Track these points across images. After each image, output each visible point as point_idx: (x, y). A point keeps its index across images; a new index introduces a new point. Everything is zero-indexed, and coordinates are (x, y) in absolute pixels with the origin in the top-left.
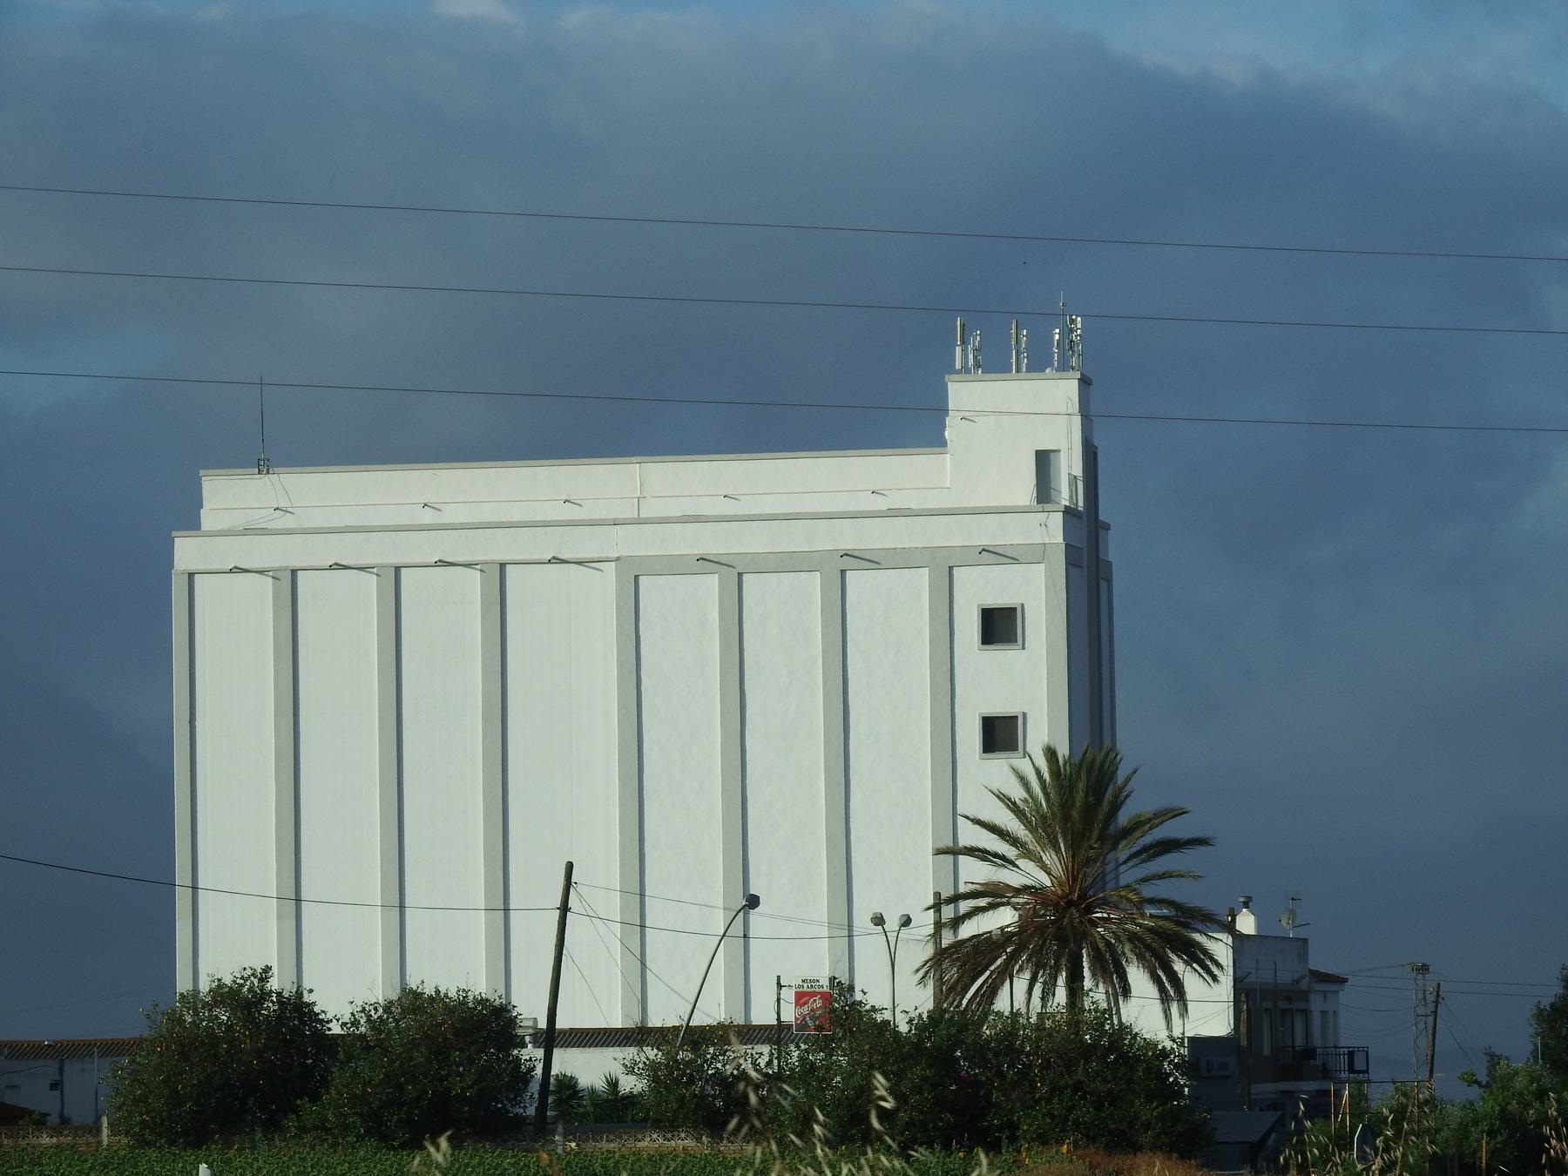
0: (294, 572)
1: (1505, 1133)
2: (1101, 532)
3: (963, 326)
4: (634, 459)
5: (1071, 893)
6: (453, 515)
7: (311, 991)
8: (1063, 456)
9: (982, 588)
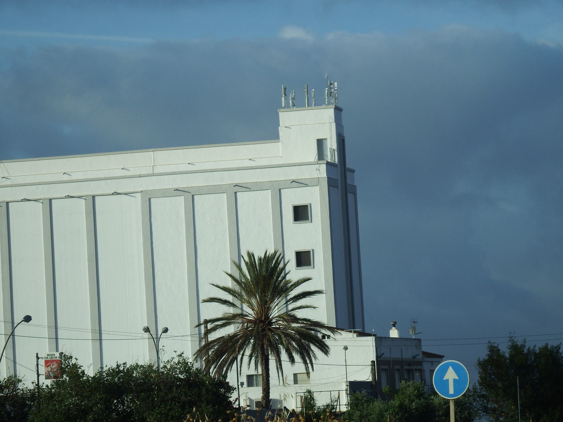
0: (7, 203)
1: (400, 414)
2: (348, 174)
3: (285, 89)
4: (151, 150)
5: (261, 317)
6: (74, 177)
7: (33, 383)
8: (328, 141)
9: (293, 198)
